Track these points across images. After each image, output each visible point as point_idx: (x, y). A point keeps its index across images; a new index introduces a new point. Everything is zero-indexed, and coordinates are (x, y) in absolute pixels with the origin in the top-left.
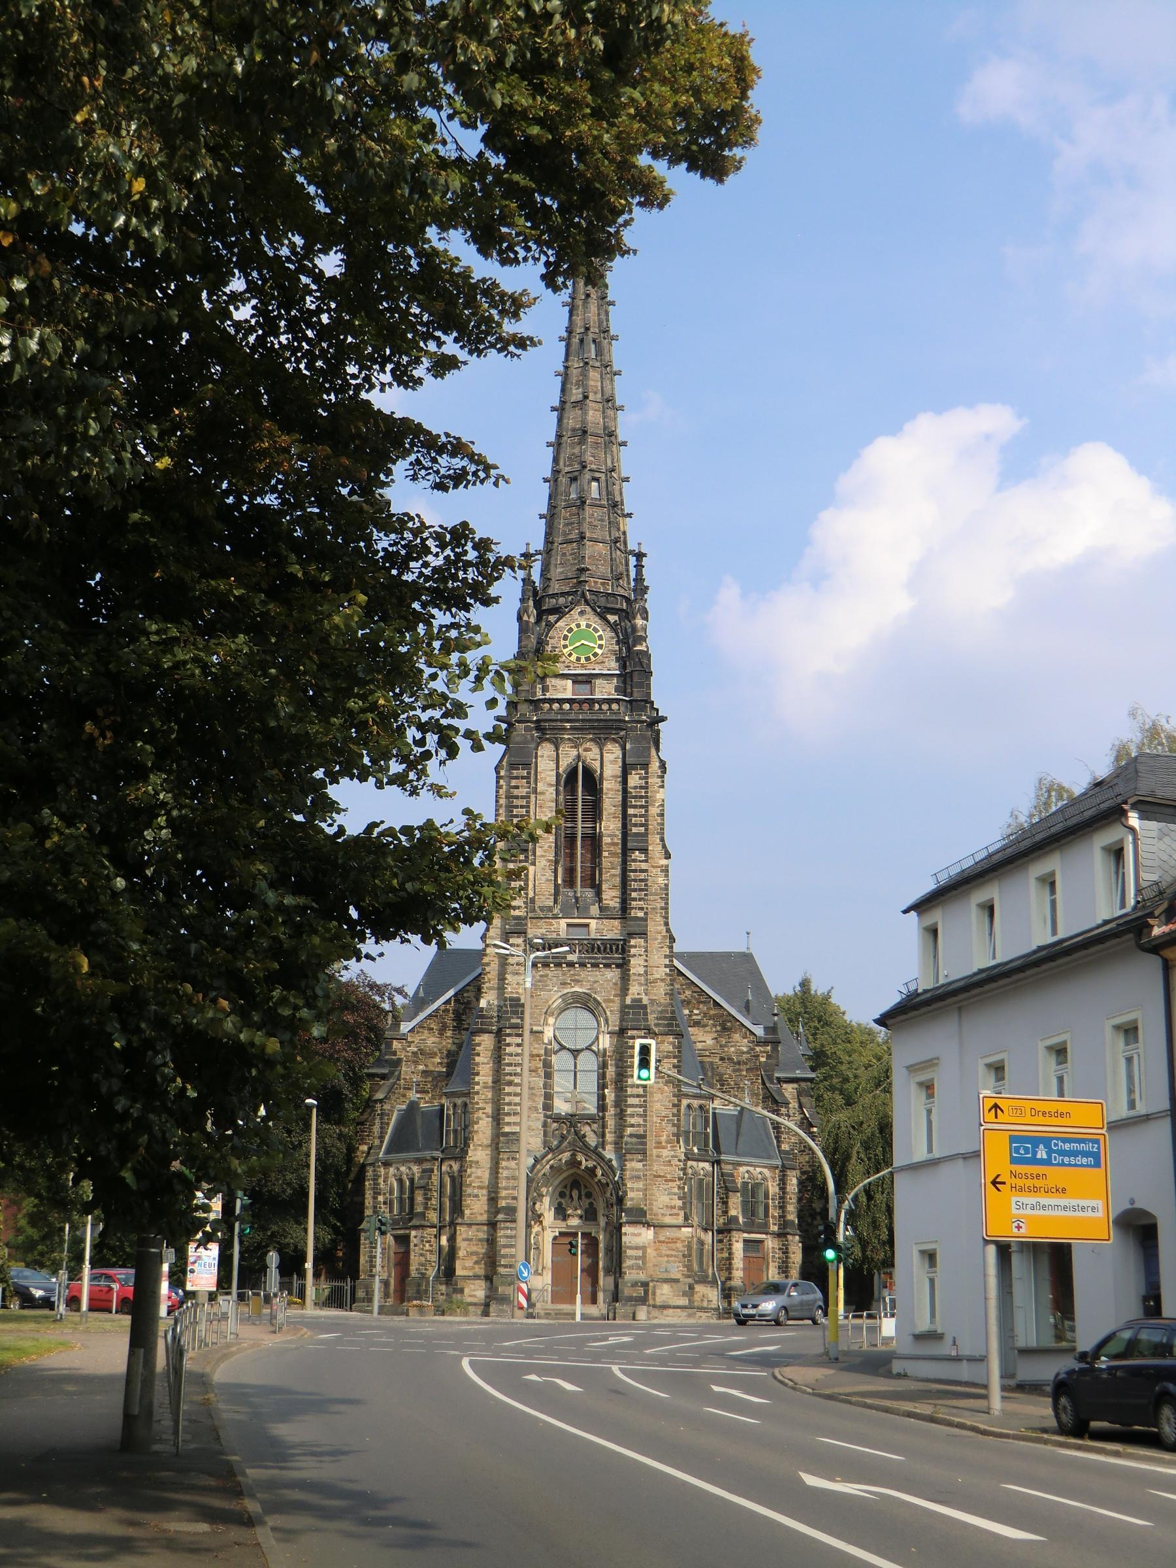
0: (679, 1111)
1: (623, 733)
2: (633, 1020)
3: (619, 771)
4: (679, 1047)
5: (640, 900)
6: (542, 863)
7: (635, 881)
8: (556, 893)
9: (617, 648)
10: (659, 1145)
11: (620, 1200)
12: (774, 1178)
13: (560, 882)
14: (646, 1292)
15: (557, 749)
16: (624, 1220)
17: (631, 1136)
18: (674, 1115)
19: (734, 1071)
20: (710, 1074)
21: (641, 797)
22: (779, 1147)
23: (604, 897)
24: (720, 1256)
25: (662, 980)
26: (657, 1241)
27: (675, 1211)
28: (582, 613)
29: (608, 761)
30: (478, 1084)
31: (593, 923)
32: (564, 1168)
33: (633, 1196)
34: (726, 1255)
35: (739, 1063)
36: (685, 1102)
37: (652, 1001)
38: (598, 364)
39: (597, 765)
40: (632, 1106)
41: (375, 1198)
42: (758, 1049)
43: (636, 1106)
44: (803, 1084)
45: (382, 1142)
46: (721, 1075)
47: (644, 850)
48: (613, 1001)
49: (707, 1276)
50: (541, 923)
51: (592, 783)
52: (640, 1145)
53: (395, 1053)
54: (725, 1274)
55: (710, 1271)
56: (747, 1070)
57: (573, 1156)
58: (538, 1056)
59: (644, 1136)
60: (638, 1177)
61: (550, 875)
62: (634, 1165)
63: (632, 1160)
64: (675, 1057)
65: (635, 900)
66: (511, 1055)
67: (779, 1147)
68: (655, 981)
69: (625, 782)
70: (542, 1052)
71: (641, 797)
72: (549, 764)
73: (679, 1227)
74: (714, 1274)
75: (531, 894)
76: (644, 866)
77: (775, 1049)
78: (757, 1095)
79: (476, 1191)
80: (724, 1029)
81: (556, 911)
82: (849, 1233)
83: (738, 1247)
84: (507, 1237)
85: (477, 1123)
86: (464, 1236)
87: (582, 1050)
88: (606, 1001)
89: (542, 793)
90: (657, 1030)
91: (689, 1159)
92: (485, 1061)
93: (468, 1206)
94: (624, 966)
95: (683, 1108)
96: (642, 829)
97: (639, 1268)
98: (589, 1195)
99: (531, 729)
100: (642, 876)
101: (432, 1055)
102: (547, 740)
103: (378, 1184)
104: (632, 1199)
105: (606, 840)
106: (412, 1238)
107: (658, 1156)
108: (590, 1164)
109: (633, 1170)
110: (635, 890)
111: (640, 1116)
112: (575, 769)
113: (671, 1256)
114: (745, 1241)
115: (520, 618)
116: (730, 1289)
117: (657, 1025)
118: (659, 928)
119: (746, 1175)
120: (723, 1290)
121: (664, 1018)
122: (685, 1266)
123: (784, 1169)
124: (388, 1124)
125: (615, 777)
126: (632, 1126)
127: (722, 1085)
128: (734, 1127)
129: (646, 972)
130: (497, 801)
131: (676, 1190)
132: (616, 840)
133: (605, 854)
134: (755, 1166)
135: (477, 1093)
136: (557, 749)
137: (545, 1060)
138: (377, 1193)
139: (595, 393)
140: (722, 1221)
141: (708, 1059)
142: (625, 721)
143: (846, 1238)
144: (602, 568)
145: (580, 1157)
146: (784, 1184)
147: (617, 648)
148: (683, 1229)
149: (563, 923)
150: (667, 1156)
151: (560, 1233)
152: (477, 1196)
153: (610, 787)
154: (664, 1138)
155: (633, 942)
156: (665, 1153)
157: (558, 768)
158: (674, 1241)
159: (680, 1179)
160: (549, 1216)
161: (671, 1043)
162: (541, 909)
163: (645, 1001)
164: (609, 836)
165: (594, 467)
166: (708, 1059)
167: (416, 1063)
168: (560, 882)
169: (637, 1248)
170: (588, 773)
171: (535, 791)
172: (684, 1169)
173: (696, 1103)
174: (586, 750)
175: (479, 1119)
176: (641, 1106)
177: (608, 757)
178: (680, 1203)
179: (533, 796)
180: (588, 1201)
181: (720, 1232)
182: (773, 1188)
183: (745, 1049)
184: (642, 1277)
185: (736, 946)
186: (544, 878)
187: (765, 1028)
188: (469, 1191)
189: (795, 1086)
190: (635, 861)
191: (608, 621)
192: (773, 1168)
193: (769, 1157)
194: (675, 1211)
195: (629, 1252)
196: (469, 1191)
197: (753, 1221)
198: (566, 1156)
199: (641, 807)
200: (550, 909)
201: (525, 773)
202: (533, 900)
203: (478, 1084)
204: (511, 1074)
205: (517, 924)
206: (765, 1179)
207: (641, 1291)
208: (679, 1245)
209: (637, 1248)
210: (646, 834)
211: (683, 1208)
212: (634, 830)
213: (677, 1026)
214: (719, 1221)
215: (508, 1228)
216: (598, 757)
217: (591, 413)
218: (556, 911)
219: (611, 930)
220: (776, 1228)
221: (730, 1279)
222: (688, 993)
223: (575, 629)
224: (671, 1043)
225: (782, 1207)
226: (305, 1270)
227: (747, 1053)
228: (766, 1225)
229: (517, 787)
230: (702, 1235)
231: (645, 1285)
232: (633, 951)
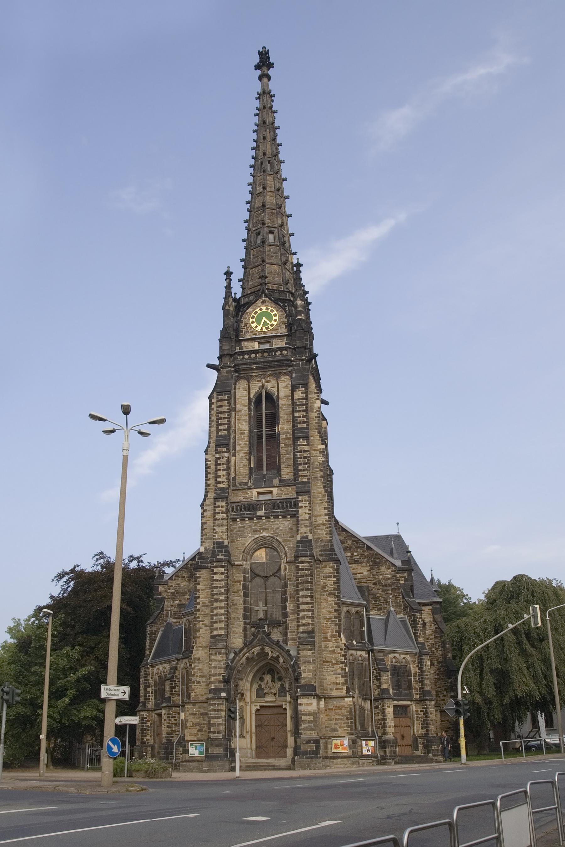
0: (339, 614)
1: (290, 368)
2: (302, 551)
3: (289, 393)
4: (337, 569)
5: (304, 470)
6: (240, 455)
7: (301, 458)
8: (251, 473)
9: (286, 320)
10: (326, 639)
11: (297, 679)
12: (414, 662)
13: (252, 466)
14: (318, 747)
15: (249, 382)
16: (299, 694)
17: (303, 632)
18: (336, 617)
19: (383, 591)
20: (366, 594)
21: (303, 405)
22: (416, 640)
23: (282, 473)
24: (377, 718)
25: (324, 524)
26: (327, 708)
27: (339, 686)
28: (263, 302)
29: (281, 387)
30: (199, 604)
31: (275, 490)
32: (256, 658)
33: (307, 674)
34: (381, 717)
35: (386, 585)
36: (345, 609)
37: (317, 540)
38: (272, 173)
39: (275, 390)
40: (303, 611)
41: (145, 690)
42: (398, 575)
43: (306, 611)
44: (435, 606)
45: (151, 652)
46: (374, 594)
47: (307, 438)
48: (289, 541)
49: (368, 733)
50: (240, 493)
51: (272, 400)
52: (309, 639)
53: (160, 594)
54: (380, 731)
55: (370, 730)
56: (392, 590)
57: (263, 649)
58: (239, 582)
59: (313, 632)
60: (309, 662)
61: (245, 462)
62: (307, 654)
63: (304, 650)
64: (334, 576)
65: (301, 470)
66: (217, 580)
67: (416, 640)
68: (318, 525)
69: (293, 399)
70: (242, 579)
71: (303, 405)
72: (243, 394)
73: (343, 697)
74: (373, 731)
75: (233, 475)
76: (306, 448)
77: (410, 575)
78: (400, 606)
79: (198, 679)
80: (375, 564)
81: (249, 485)
82: (466, 691)
83: (390, 711)
84: (215, 710)
85: (199, 631)
86: (190, 712)
87: (271, 576)
88: (284, 541)
89: (240, 411)
90: (321, 558)
91: (349, 649)
92: (204, 588)
93: (193, 690)
94: (294, 515)
95: (343, 615)
96: (305, 425)
97: (311, 729)
98: (280, 679)
99: (231, 372)
100: (306, 454)
101: (184, 594)
102: (242, 378)
103: (148, 680)
104: (305, 678)
105: (283, 436)
106: (163, 716)
107: (325, 647)
108: (275, 654)
109: (304, 657)
110: (301, 464)
111: (308, 617)
112: (261, 395)
113: (338, 719)
114: (395, 707)
115: (224, 308)
116: (385, 741)
117: (321, 555)
118: (320, 490)
119: (394, 660)
120: (380, 742)
121: (325, 550)
122: (348, 726)
123: (421, 654)
124: (155, 640)
125: (287, 396)
126: (304, 625)
127: (376, 601)
128: (382, 627)
129: (310, 518)
130: (210, 418)
131: (339, 671)
132: (289, 436)
133: (282, 445)
134: (400, 654)
135: (198, 610)
136: (249, 382)
137: (244, 584)
138: (147, 686)
139: (270, 187)
140: (377, 693)
141: (365, 585)
142: (291, 361)
143: (464, 696)
144: (277, 279)
145: (267, 650)
146: (422, 665)
147: (286, 320)
148: (346, 699)
149: (255, 492)
150: (334, 645)
151: (261, 707)
152: (199, 683)
153: (284, 403)
154: (329, 634)
155: (300, 498)
156: (331, 644)
157: (249, 394)
158: (340, 708)
159: (342, 663)
160: (250, 693)
161: (332, 567)
162: (240, 484)
163: (310, 537)
164: (284, 433)
165: (270, 225)
166: (365, 585)
167: (174, 599)
168: (252, 466)
169: (309, 714)
170: (269, 396)
171: (235, 410)
172: (345, 656)
173: (353, 610)
174: (268, 382)
175: (200, 628)
176: (309, 611)
177: (282, 385)
178: (343, 680)
179: (233, 413)
180: (280, 683)
181: (376, 700)
182: (414, 669)
183: (389, 576)
184: (314, 736)
185: (391, 531)
186: (241, 465)
187: (403, 562)
188: (193, 679)
189: (430, 607)
190: (300, 445)
191: (280, 305)
192: (412, 654)
193: (410, 647)
194: (339, 686)
195: (304, 718)
196: (193, 679)
197: (401, 693)
198: (257, 650)
199: (303, 411)
200: (246, 484)
201: (226, 397)
202: (234, 479)
203: (199, 604)
204: (217, 594)
205: (221, 493)
206: (407, 662)
207: (314, 746)
208: (344, 711)
209: (309, 714)
210: (307, 428)
211: (346, 683)
212: (299, 426)
213: (335, 555)
214: (376, 693)
215: (215, 704)
216: (276, 385)
217: (268, 197)
218: (249, 485)
219: (288, 493)
220: (418, 697)
221: (384, 734)
222: (349, 542)
223: (259, 312)
224: (332, 567)
225: (421, 681)
226: (40, 740)
227: (391, 578)
228: (411, 695)
229: (221, 406)
230: (363, 704)
231: (316, 741)
232: (301, 504)
